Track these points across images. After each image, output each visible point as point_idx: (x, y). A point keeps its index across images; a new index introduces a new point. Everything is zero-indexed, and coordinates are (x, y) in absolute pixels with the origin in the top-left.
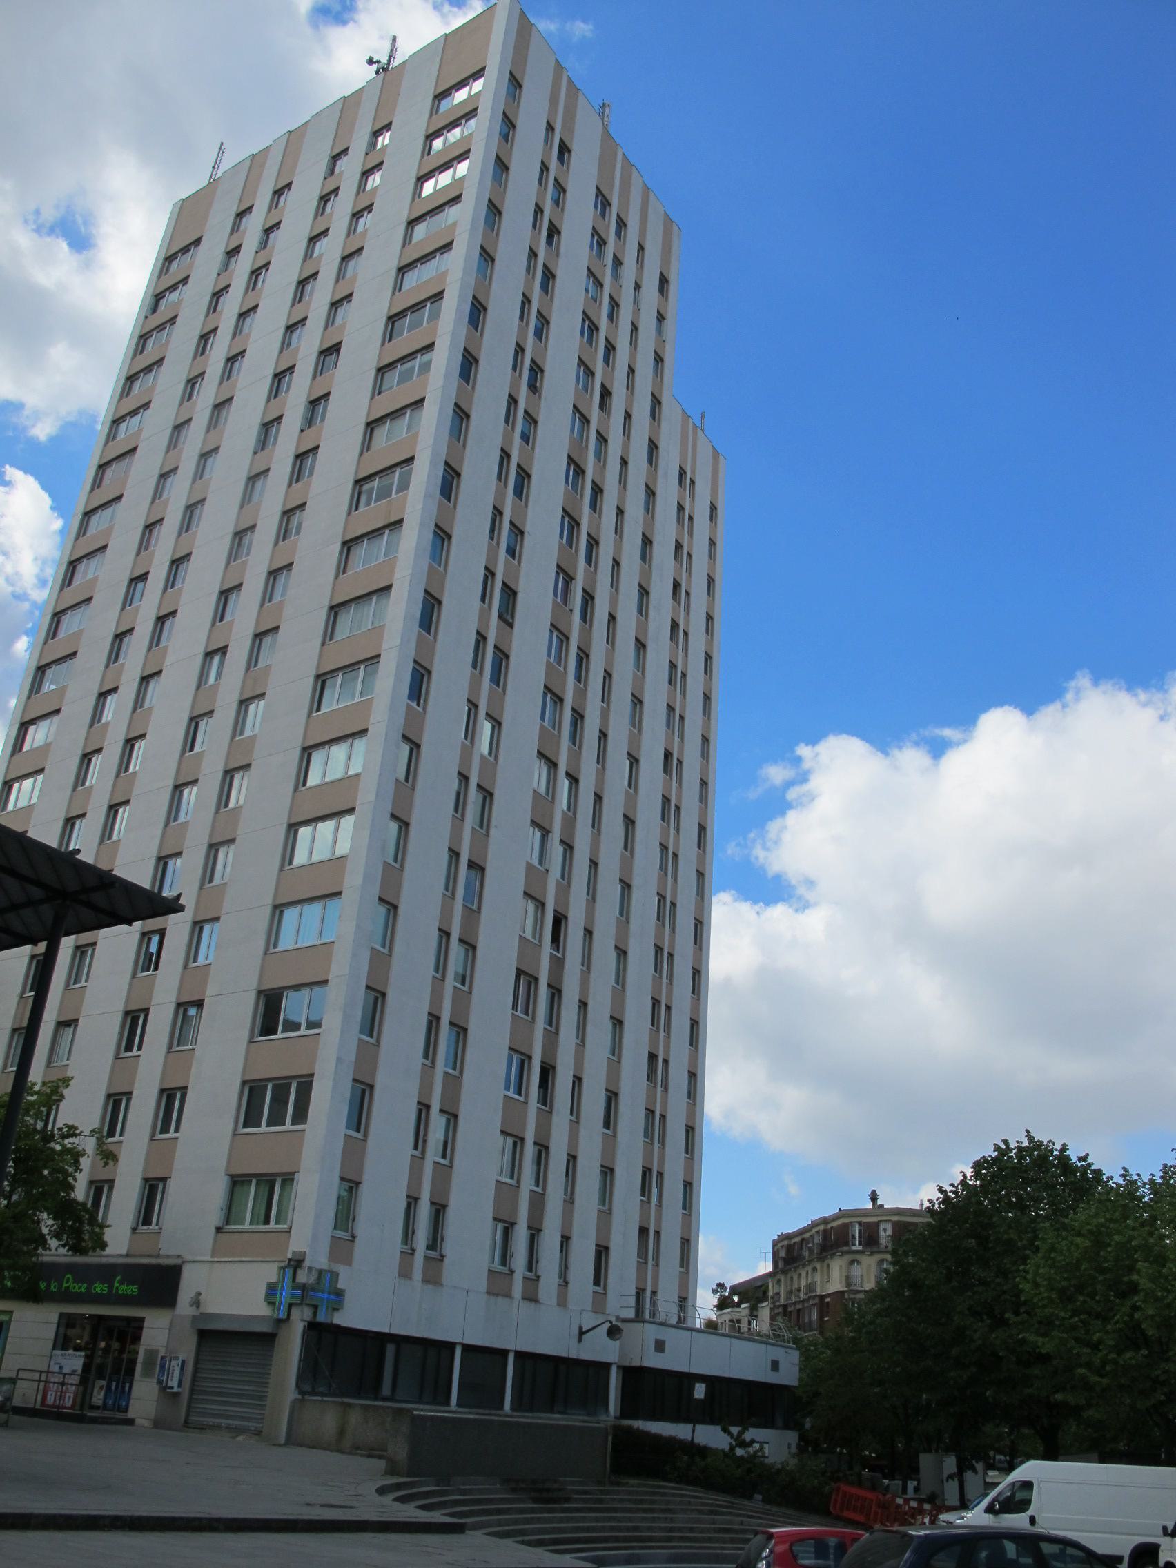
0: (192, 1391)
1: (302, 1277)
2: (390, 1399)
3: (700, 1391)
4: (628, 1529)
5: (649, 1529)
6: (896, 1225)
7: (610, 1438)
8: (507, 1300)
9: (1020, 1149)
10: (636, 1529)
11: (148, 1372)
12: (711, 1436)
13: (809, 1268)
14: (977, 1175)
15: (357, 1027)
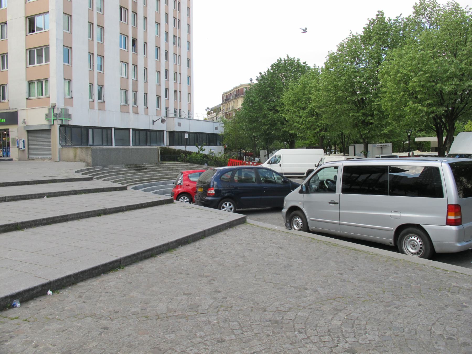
0: (28, 149)
1: (56, 111)
2: (93, 145)
3: (186, 136)
4: (164, 175)
5: (171, 175)
8: (128, 114)
9: (285, 60)
10: (167, 175)
11: (14, 145)
12: (193, 149)
13: (232, 102)
14: (272, 69)
15: (62, 28)
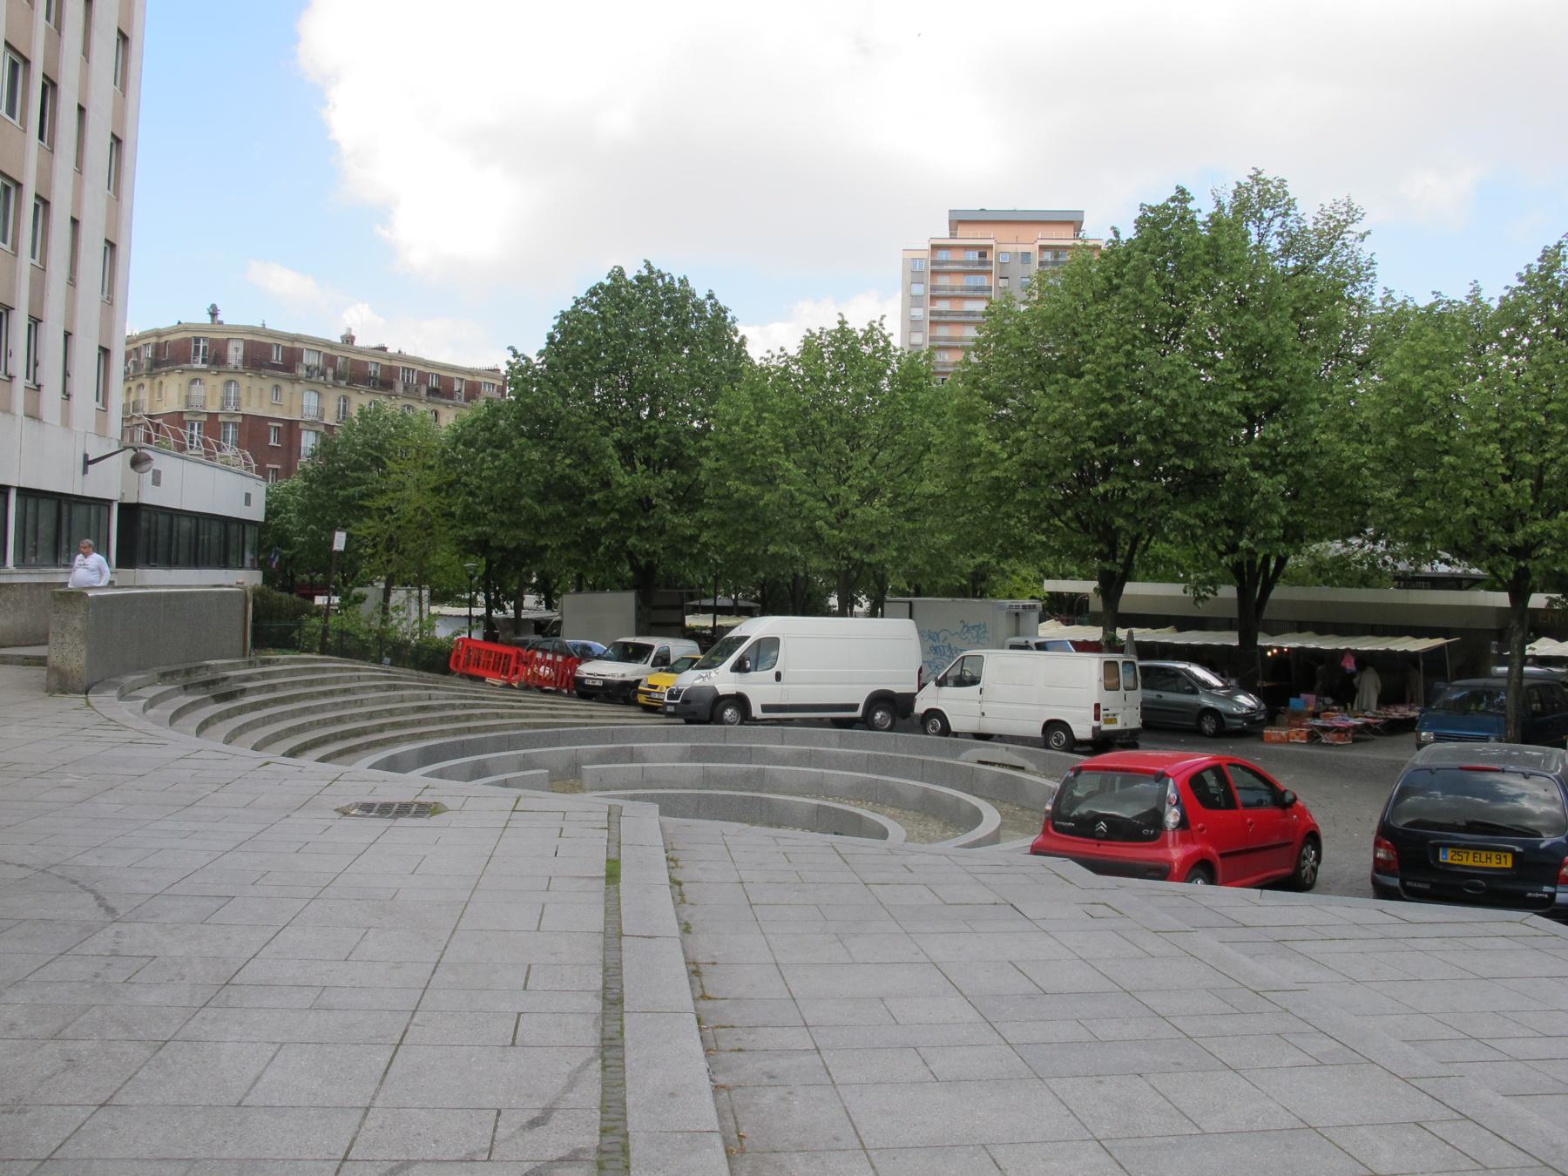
6: (246, 343)
7: (250, 606)
8: (8, 417)
